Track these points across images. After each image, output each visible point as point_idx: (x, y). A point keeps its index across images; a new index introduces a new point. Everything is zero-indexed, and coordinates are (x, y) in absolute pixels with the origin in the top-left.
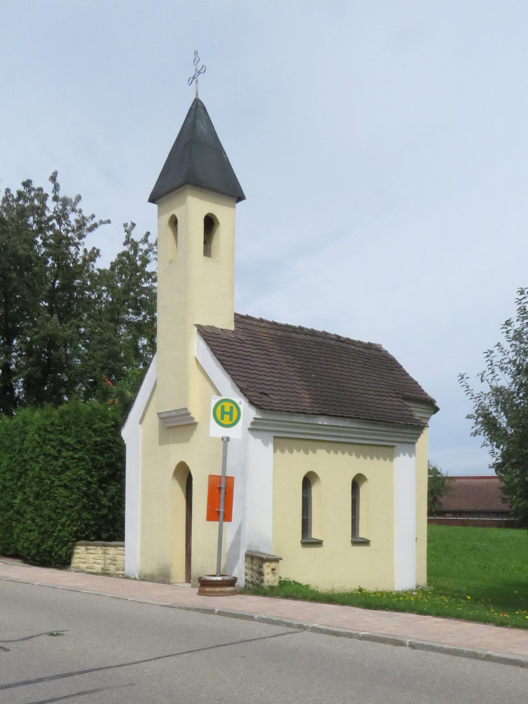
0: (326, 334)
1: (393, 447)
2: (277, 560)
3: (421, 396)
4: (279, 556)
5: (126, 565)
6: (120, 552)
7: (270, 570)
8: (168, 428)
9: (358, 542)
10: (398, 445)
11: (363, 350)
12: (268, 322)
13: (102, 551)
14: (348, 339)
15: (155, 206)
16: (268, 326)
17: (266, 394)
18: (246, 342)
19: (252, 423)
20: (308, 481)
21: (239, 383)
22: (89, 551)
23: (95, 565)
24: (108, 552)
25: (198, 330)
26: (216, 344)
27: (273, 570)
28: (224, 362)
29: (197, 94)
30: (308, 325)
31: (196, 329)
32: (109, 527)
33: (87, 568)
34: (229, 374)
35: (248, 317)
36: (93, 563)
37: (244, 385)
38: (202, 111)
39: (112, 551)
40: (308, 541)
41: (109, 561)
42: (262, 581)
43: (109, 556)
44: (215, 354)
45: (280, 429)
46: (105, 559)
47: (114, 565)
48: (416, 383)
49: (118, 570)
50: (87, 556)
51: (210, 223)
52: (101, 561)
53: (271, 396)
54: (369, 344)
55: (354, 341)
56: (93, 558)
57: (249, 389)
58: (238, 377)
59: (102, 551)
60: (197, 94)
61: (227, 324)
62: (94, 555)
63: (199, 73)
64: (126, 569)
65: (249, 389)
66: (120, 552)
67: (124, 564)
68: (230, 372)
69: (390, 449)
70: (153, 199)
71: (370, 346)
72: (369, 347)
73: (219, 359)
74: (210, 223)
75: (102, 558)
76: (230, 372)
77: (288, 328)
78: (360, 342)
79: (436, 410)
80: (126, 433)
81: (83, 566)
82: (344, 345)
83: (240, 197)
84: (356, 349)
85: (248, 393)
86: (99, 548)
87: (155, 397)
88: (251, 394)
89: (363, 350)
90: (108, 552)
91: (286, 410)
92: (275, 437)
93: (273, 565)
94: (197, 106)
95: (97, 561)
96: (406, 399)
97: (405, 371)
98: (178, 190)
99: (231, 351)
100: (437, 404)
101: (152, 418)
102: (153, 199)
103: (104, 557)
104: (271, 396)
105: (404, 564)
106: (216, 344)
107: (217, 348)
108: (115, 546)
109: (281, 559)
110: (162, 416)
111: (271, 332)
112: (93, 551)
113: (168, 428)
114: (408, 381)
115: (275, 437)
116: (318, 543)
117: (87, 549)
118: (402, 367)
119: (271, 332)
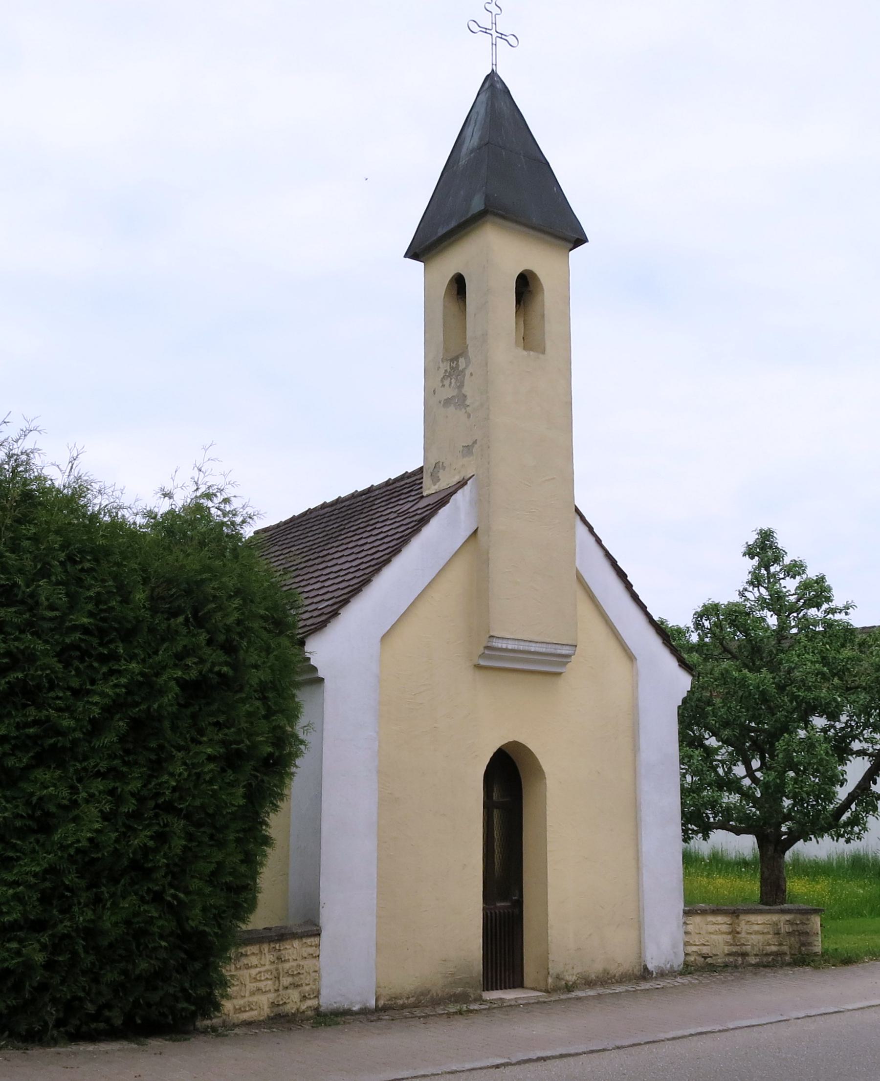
15: (418, 266)
20: (509, 778)
23: (254, 999)
36: (253, 994)
41: (286, 981)
49: (304, 998)
51: (526, 286)
52: (269, 985)
62: (254, 972)
64: (323, 992)
70: (416, 252)
74: (526, 286)
83: (580, 240)
86: (266, 947)
94: (492, 86)
102: (416, 252)
112: (254, 960)
113: (478, 667)
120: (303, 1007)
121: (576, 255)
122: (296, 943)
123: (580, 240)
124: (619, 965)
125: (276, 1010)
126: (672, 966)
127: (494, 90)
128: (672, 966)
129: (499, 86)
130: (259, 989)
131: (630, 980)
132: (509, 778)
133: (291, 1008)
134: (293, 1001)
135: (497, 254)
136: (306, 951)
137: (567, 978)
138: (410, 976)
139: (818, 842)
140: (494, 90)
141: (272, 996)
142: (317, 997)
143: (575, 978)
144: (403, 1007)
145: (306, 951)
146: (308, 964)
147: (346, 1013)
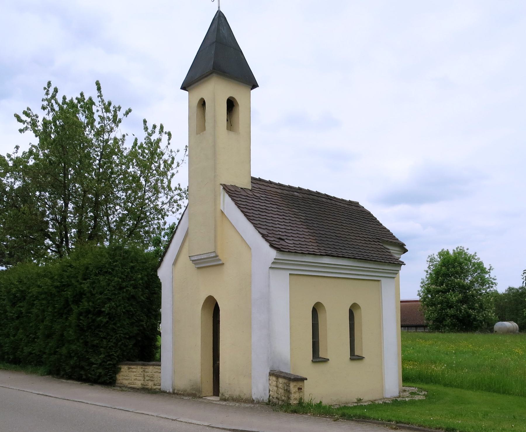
0: (319, 193)
1: (379, 281)
2: (303, 379)
6: (157, 370)
7: (296, 389)
8: (198, 268)
9: (355, 357)
10: (383, 280)
11: (346, 206)
12: (275, 184)
13: (142, 370)
14: (335, 198)
15: (186, 93)
16: (275, 186)
17: (283, 240)
18: (261, 198)
19: (273, 263)
22: (131, 370)
23: (136, 381)
25: (224, 188)
26: (239, 199)
27: (300, 389)
28: (247, 214)
29: (219, 7)
30: (305, 186)
31: (222, 187)
32: (145, 348)
33: (129, 383)
34: (252, 223)
35: (260, 180)
36: (135, 380)
38: (223, 19)
39: (150, 369)
40: (317, 357)
41: (147, 378)
42: (289, 398)
43: (148, 374)
46: (144, 376)
47: (152, 381)
48: (389, 231)
49: (155, 385)
50: (131, 374)
51: (231, 104)
53: (286, 240)
54: (350, 201)
55: (339, 199)
56: (134, 376)
57: (269, 235)
58: (259, 226)
59: (142, 370)
60: (219, 7)
61: (245, 184)
62: (135, 373)
64: (162, 384)
65: (269, 235)
66: (157, 370)
67: (160, 380)
68: (252, 221)
69: (376, 283)
70: (185, 87)
71: (350, 203)
72: (350, 204)
73: (242, 211)
74: (231, 104)
75: (142, 375)
76: (252, 221)
77: (290, 188)
78: (343, 200)
79: (406, 251)
80: (164, 273)
81: (126, 382)
83: (255, 85)
84: (342, 205)
85: (268, 238)
86: (139, 367)
87: (186, 244)
89: (346, 206)
91: (307, 252)
92: (290, 274)
93: (299, 384)
94: (219, 16)
95: (138, 378)
97: (379, 222)
98: (206, 79)
99: (251, 205)
100: (406, 247)
101: (184, 259)
102: (185, 87)
103: (144, 374)
104: (286, 240)
106: (239, 199)
107: (240, 202)
108: (153, 365)
109: (306, 379)
110: (193, 259)
111: (279, 191)
112: (134, 370)
113: (198, 268)
114: (383, 230)
115: (290, 274)
116: (326, 360)
117: (129, 368)
118: (376, 219)
119: (279, 191)
121: (254, 92)
123: (255, 85)
124: (245, 394)
125: (143, 386)
126: (263, 400)
127: (220, 22)
128: (263, 400)
129: (221, 14)
130: (136, 379)
131: (249, 403)
132: (213, 309)
134: (150, 385)
137: (226, 396)
138: (182, 384)
140: (220, 22)
141: (142, 382)
142: (160, 385)
143: (228, 396)
144: (180, 394)
146: (156, 374)
147: (165, 392)
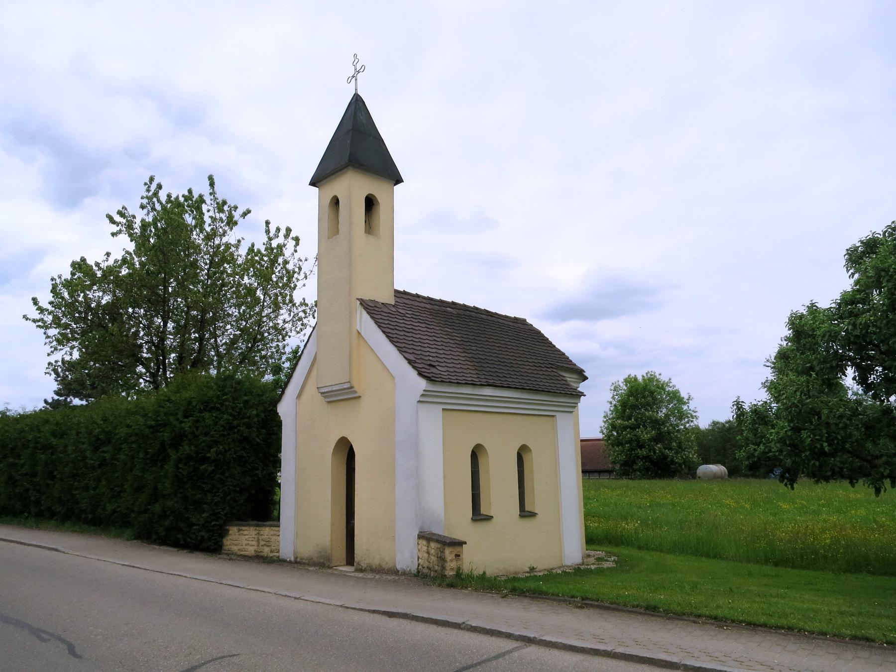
2: (461, 544)
3: (571, 366)
4: (462, 539)
5: (281, 546)
7: (453, 556)
8: (329, 402)
9: (525, 513)
11: (511, 324)
12: (424, 298)
13: (255, 532)
19: (423, 395)
20: (476, 455)
21: (407, 355)
24: (262, 533)
29: (356, 90)
32: (262, 506)
37: (411, 357)
39: (266, 531)
40: (478, 515)
41: (262, 543)
44: (379, 327)
45: (476, 403)
46: (258, 540)
49: (272, 552)
51: (370, 203)
52: (254, 543)
54: (515, 318)
58: (404, 349)
59: (255, 532)
60: (356, 90)
63: (359, 72)
69: (551, 419)
70: (313, 183)
71: (516, 320)
74: (370, 203)
82: (494, 319)
83: (398, 180)
85: (416, 365)
86: (252, 528)
88: (421, 366)
89: (511, 324)
90: (262, 533)
92: (443, 409)
93: (457, 550)
94: (357, 100)
96: (557, 367)
97: (551, 343)
101: (311, 390)
102: (313, 183)
105: (562, 536)
108: (271, 526)
109: (465, 543)
110: (323, 390)
112: (246, 532)
113: (329, 402)
115: (443, 409)
116: (489, 518)
117: (239, 530)
119: (428, 306)
120: (272, 555)
121: (397, 188)
122: (267, 529)
123: (398, 180)
132: (347, 454)
133: (265, 554)
134: (266, 551)
135: (353, 187)
136: (272, 533)
138: (307, 550)
139: (35, 301)
141: (255, 548)
145: (272, 533)
146: (273, 538)
147: (284, 561)
